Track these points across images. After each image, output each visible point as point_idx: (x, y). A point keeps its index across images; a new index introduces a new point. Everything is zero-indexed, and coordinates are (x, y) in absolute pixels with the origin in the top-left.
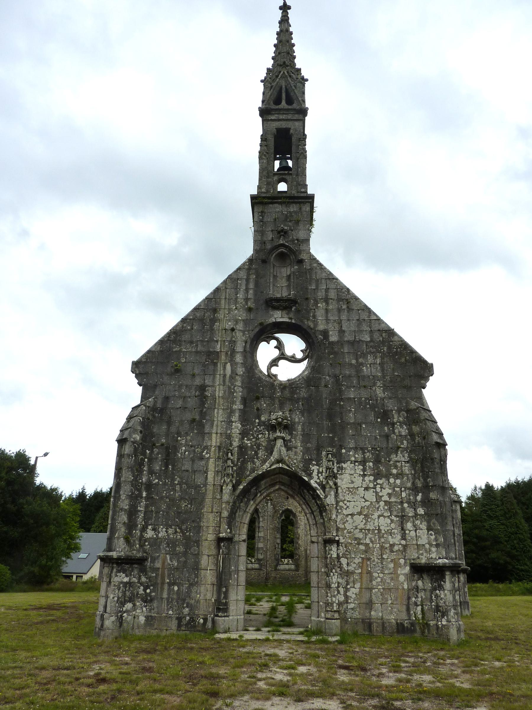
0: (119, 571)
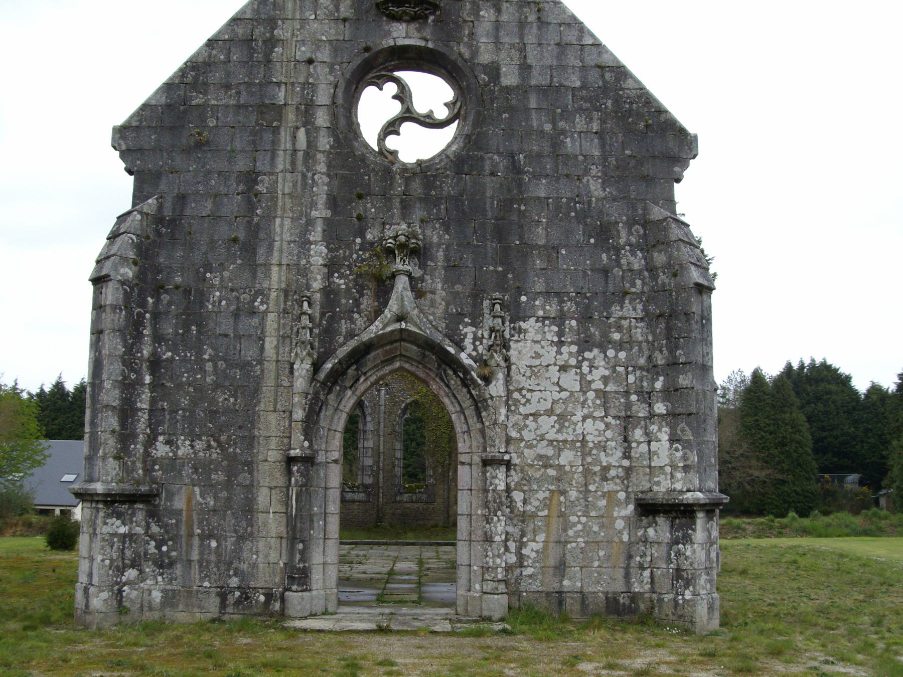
0: (108, 516)
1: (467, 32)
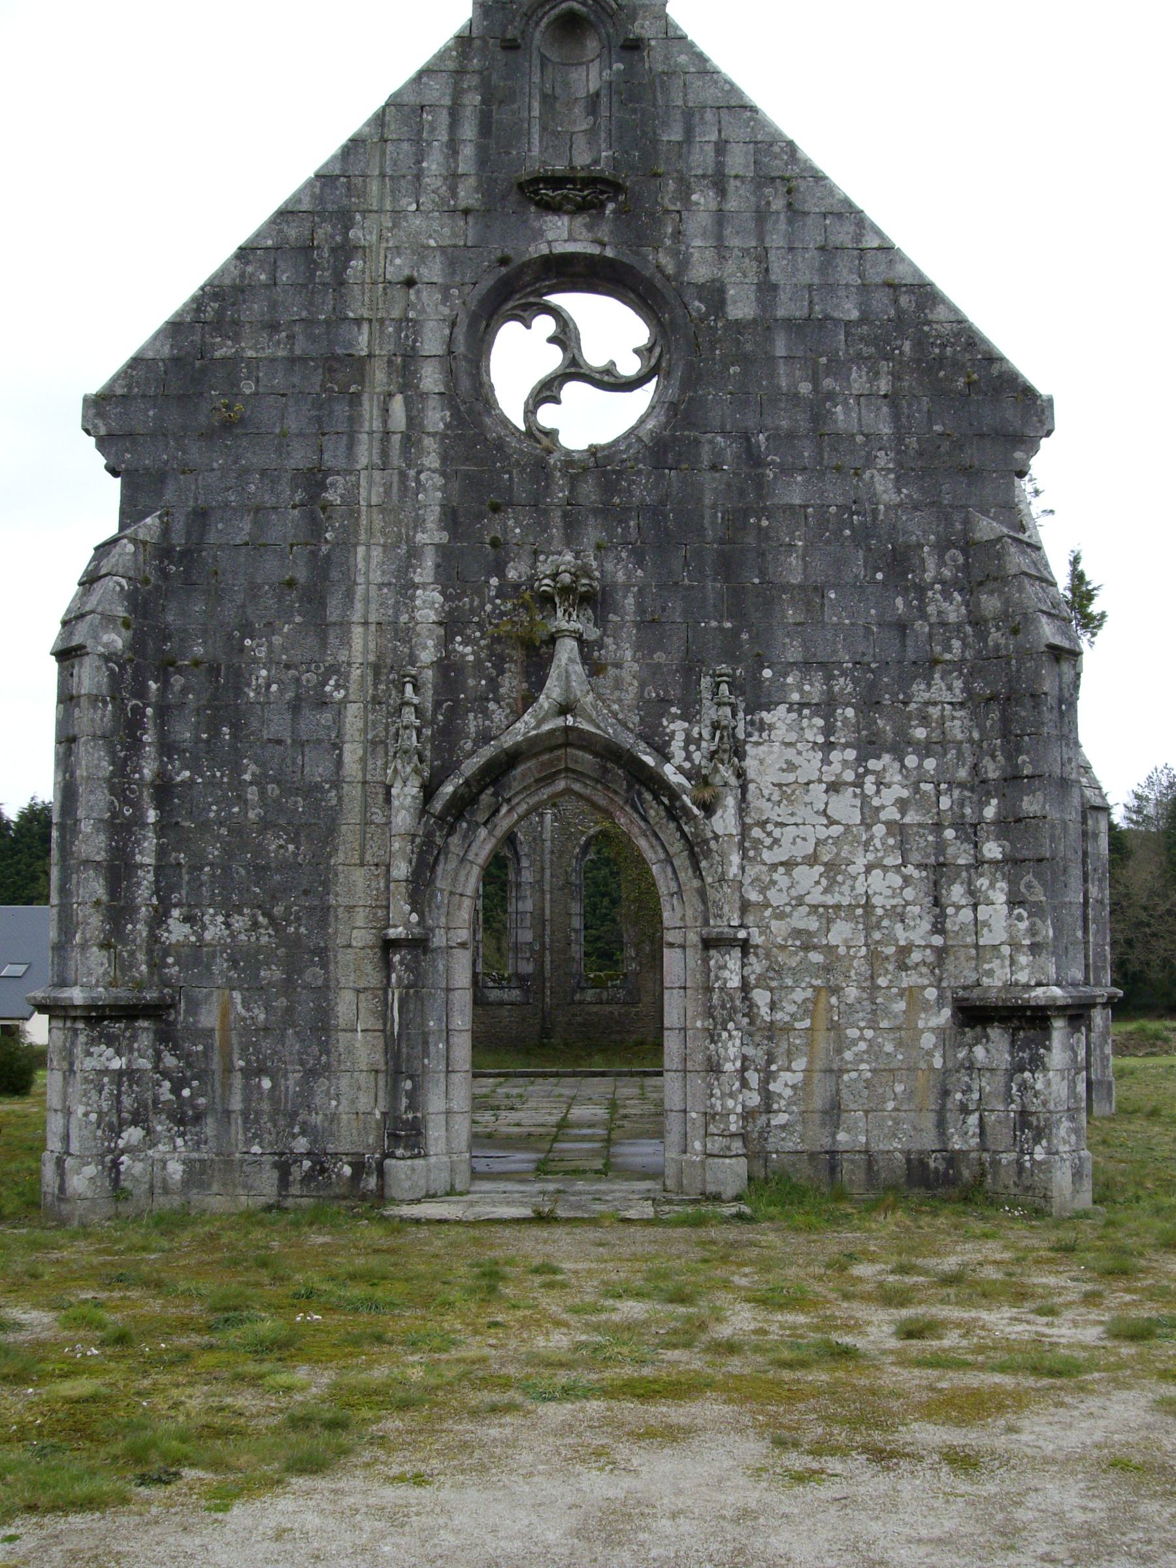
0: (93, 1041)
1: (670, 230)
